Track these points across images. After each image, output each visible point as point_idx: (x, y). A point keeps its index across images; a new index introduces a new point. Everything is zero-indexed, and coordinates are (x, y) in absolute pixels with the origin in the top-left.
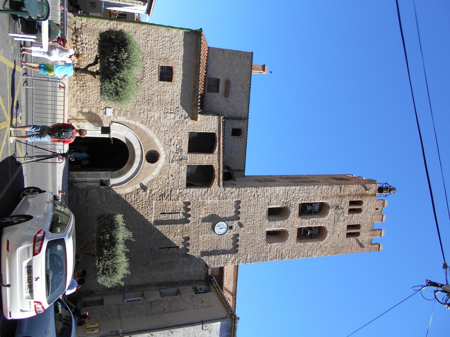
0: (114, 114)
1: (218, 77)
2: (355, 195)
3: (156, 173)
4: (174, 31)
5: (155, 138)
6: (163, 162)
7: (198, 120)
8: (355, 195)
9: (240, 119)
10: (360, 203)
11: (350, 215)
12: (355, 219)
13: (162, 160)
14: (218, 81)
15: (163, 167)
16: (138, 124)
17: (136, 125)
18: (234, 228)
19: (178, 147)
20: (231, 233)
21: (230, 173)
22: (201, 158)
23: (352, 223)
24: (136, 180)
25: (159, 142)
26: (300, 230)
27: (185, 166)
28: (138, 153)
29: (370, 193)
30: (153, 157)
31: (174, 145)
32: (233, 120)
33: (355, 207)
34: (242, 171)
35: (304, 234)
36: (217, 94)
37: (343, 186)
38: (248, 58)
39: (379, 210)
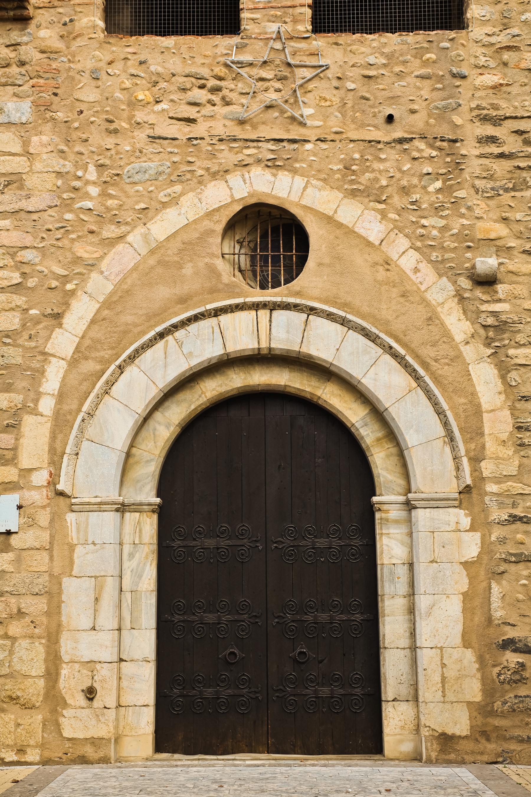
4: (72, 474)
5: (146, 237)
6: (299, 182)
13: (282, 189)
17: (68, 351)
19: (202, 95)
24: (415, 338)
25: (171, 213)
28: (241, 333)
30: (273, 239)
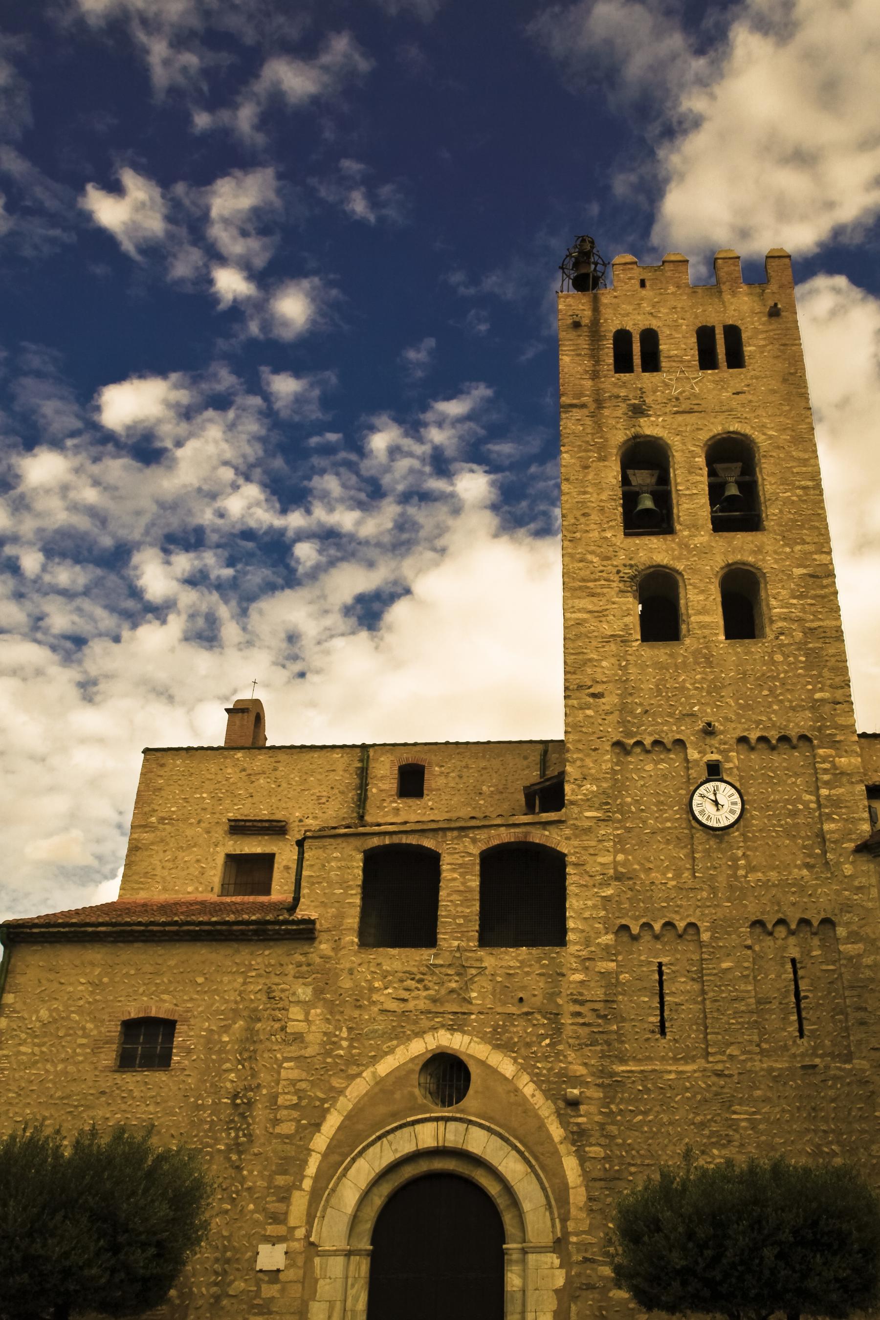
0: (280, 1239)
1: (220, 860)
2: (596, 359)
3: (507, 1067)
5: (374, 1074)
6: (467, 1038)
7: (314, 916)
8: (596, 359)
9: (363, 775)
10: (622, 338)
11: (664, 364)
12: (679, 345)
14: (232, 859)
15: (484, 1038)
16: (320, 1142)
18: (715, 757)
20: (734, 760)
21: (542, 790)
22: (455, 897)
23: (692, 355)
25: (389, 1059)
26: (720, 525)
27: (481, 953)
28: (427, 1136)
29: (588, 313)
30: (448, 1076)
31: (404, 1000)
32: (366, 798)
33: (637, 352)
34: (546, 752)
35: (737, 509)
36: (277, 859)
37: (564, 400)
38: (162, 765)
39: (647, 275)
